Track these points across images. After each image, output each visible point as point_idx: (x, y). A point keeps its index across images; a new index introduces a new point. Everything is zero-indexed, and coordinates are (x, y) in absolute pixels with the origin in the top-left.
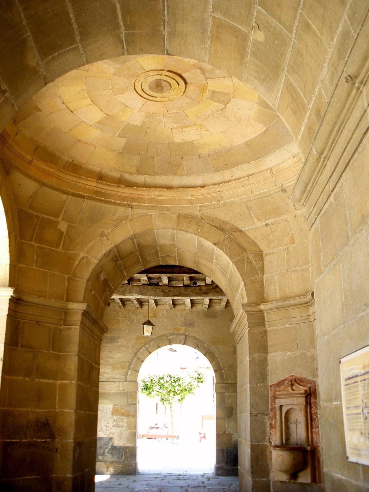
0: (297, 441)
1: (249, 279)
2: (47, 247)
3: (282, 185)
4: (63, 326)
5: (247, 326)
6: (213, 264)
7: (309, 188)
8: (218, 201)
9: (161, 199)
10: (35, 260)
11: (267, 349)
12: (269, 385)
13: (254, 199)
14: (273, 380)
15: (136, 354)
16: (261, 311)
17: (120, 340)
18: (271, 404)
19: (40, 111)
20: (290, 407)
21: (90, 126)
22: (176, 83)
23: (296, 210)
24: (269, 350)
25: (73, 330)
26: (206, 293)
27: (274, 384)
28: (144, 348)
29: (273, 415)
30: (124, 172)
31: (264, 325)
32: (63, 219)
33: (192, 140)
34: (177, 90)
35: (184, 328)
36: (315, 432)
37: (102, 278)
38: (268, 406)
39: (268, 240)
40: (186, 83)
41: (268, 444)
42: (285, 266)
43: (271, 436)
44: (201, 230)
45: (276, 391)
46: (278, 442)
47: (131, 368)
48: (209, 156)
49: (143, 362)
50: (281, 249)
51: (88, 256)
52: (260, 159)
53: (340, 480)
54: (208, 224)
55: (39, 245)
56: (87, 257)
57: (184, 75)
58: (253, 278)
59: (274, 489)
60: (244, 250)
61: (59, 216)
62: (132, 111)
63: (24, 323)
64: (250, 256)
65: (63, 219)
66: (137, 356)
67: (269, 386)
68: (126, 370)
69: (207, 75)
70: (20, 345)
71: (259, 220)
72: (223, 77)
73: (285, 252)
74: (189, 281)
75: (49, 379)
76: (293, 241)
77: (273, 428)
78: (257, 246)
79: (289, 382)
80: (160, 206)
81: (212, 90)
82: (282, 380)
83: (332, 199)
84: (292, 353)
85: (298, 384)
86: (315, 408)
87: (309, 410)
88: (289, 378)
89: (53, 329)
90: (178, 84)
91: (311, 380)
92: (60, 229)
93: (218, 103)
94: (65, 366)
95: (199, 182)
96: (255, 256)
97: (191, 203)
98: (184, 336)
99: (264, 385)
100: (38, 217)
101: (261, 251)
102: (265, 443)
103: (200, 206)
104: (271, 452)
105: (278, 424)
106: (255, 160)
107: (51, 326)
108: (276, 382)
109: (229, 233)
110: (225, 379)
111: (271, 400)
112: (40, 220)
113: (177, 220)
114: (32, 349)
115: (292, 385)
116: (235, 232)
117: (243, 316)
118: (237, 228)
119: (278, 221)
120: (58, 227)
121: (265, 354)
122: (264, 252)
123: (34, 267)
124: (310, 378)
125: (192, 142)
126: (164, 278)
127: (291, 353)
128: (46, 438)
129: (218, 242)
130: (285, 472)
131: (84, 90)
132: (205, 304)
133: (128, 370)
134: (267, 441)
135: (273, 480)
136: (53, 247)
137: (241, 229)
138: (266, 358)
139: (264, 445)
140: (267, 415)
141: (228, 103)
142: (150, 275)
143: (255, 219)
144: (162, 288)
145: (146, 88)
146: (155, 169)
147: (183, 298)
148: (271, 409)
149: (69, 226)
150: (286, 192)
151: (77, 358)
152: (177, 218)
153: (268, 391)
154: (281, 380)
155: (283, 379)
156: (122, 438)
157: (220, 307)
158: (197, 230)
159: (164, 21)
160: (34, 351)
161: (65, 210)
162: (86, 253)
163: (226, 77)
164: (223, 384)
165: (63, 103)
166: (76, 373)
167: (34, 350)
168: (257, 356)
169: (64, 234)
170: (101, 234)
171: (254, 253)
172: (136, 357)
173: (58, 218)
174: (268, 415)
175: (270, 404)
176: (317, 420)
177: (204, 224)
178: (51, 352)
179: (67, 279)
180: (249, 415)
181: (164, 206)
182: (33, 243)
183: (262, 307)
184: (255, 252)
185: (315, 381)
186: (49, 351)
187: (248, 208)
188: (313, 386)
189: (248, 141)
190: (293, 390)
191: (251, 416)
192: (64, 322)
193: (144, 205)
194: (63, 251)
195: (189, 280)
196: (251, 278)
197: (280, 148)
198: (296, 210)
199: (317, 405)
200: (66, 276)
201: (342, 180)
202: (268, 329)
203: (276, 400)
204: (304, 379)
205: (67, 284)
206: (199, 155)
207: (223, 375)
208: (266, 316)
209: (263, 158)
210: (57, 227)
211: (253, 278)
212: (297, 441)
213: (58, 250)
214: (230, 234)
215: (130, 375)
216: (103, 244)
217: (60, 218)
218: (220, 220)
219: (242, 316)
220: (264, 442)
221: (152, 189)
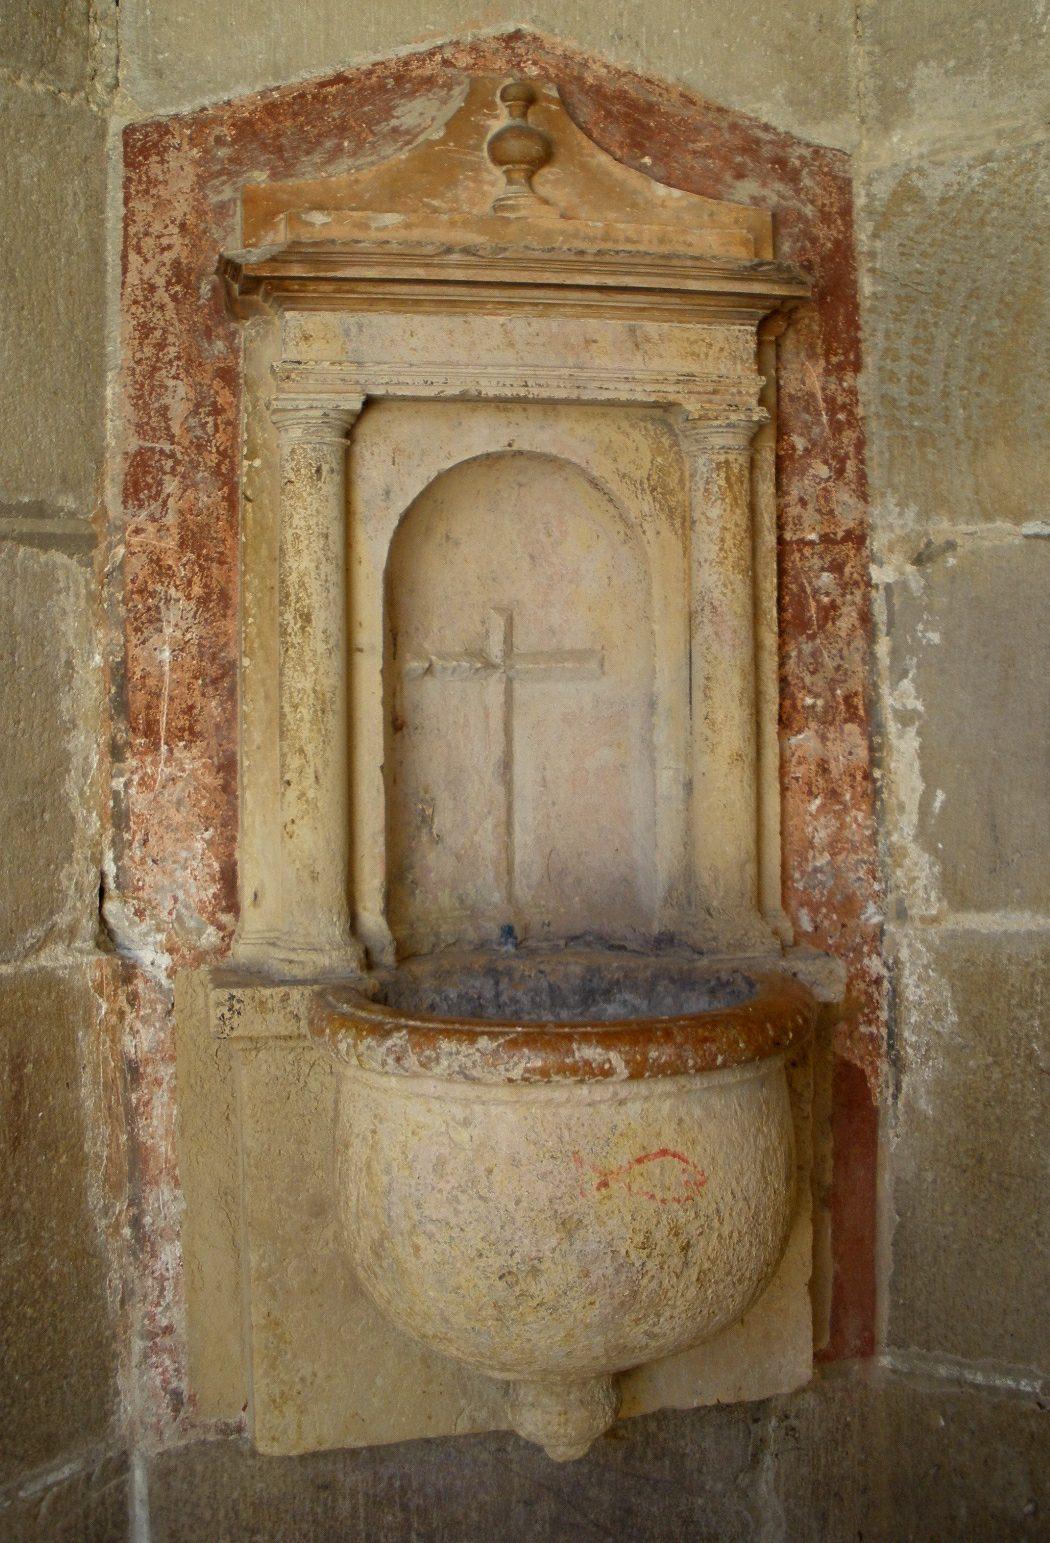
0: (510, 897)
27: (200, 123)
29: (171, 543)
36: (823, 768)
38: (95, 413)
43: (120, 846)
67: (114, 144)
77: (150, 730)
82: (340, 78)
86: (840, 472)
91: (789, 140)
99: (54, 96)
102: (44, 960)
108: (244, 92)
111: (145, 330)
124: (771, 111)
135: (173, 1441)
139: (48, 981)
140: (81, 544)
153: (97, 204)
154: (328, 72)
155: (360, 60)
174: (92, 541)
175: (114, 391)
176: (847, 620)
185: (844, 156)
188: (809, 211)
199: (860, 444)
204: (688, 113)
212: (510, 897)
220: (37, 948)
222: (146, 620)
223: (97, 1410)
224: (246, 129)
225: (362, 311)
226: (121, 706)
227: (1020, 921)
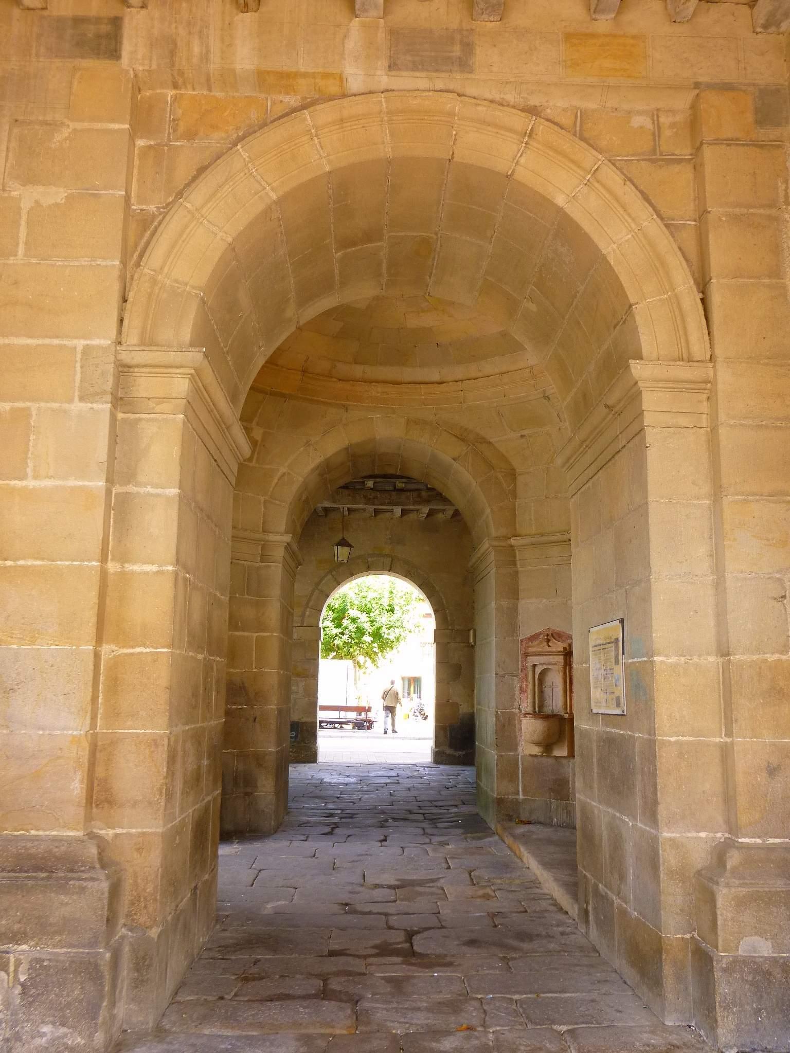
7: (571, 461)
14: (526, 632)
15: (318, 584)
16: (512, 546)
18: (522, 663)
20: (545, 667)
24: (521, 595)
26: (427, 501)
28: (330, 576)
31: (515, 565)
32: (258, 424)
38: (518, 665)
41: (517, 711)
45: (528, 647)
46: (529, 709)
53: (586, 730)
56: (289, 473)
59: (522, 764)
60: (491, 467)
64: (500, 476)
66: (320, 587)
71: (512, 430)
79: (544, 636)
83: (590, 484)
85: (555, 639)
87: (568, 671)
92: (253, 437)
94: (263, 614)
95: (436, 377)
101: (514, 470)
104: (521, 721)
105: (530, 687)
108: (529, 636)
115: (548, 641)
116: (481, 443)
122: (517, 470)
128: (242, 705)
130: (538, 744)
134: (516, 708)
138: (517, 605)
140: (517, 676)
148: (522, 669)
156: (297, 709)
157: (443, 516)
159: (431, 273)
164: (447, 631)
169: (259, 444)
172: (317, 589)
173: (252, 423)
178: (247, 596)
179: (262, 501)
180: (494, 675)
183: (512, 542)
190: (549, 646)
191: (496, 677)
194: (257, 465)
201: (599, 474)
202: (520, 569)
203: (528, 658)
205: (263, 509)
208: (517, 553)
213: (251, 465)
214: (474, 445)
216: (309, 456)
217: (254, 423)
218: (461, 427)
221: (374, 384)
222: (523, 682)
223: (516, 749)
224: (529, 639)
225: (736, 814)
226: (521, 690)
227: (787, 840)
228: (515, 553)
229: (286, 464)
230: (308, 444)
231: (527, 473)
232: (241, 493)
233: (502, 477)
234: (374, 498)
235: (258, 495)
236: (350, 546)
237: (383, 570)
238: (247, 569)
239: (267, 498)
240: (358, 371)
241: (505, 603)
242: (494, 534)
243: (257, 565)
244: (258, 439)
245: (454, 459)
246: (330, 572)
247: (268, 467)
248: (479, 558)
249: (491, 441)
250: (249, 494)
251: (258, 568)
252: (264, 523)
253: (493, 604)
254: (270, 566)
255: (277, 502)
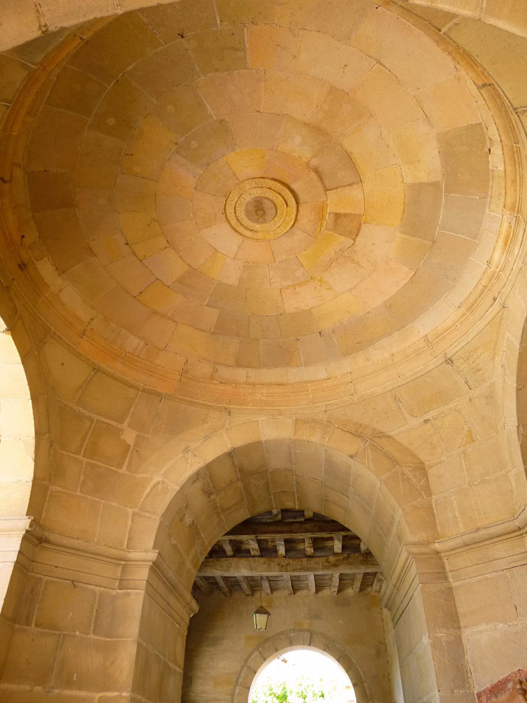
1: (409, 504)
2: (103, 465)
3: (445, 354)
4: (119, 591)
5: (417, 580)
6: (348, 497)
8: (351, 395)
9: (270, 400)
10: (81, 482)
11: (458, 621)
12: (475, 693)
13: (404, 383)
15: (246, 661)
16: (437, 553)
17: (225, 641)
19: (95, 255)
21: (168, 287)
22: (284, 202)
23: (471, 389)
25: (133, 597)
27: (485, 691)
28: (256, 653)
30: (218, 363)
31: (446, 578)
32: (130, 426)
33: (310, 307)
34: (285, 215)
35: (309, 621)
37: (188, 520)
39: (431, 444)
40: (297, 202)
42: (465, 479)
44: (329, 438)
47: (239, 684)
48: (334, 332)
49: (256, 673)
50: (453, 454)
51: (165, 481)
52: (407, 327)
54: (339, 430)
55: (90, 461)
56: (163, 482)
57: (294, 187)
58: (415, 503)
60: (395, 462)
61: (124, 421)
62: (224, 260)
63: (47, 582)
64: (407, 471)
65: (130, 426)
66: (248, 664)
67: (476, 696)
68: (232, 687)
69: (327, 182)
70: (34, 622)
71: (413, 416)
72: (349, 185)
73: (460, 458)
74: (312, 549)
75: (80, 689)
76: (472, 438)
78: (414, 456)
80: (270, 409)
81: (335, 211)
82: (499, 681)
84: (509, 626)
88: (514, 675)
89: (100, 595)
90: (287, 204)
93: (343, 237)
94: (113, 663)
96: (412, 469)
97: (312, 402)
98: (309, 634)
100: (91, 420)
101: (422, 463)
103: (326, 405)
106: (399, 330)
107: (97, 588)
108: (488, 685)
109: (370, 439)
110: (369, 697)
112: (94, 424)
113: (294, 426)
114: (56, 630)
116: (379, 437)
117: (406, 566)
118: (381, 433)
119: (443, 412)
120: (122, 437)
121: (457, 630)
122: (427, 463)
123: (78, 493)
125: (309, 312)
126: (279, 544)
127: (507, 626)
129: (356, 454)
131: (154, 220)
132: (333, 586)
133: (235, 686)
136: (113, 466)
137: (387, 434)
138: (460, 637)
141: (357, 235)
142: (261, 535)
143: (407, 416)
144: (278, 560)
145: (242, 215)
146: (261, 358)
147: (306, 573)
149: (138, 436)
150: (452, 363)
151: (135, 647)
152: (294, 423)
154: (497, 681)
155: (501, 678)
157: (352, 591)
158: (324, 438)
160: (60, 635)
161: (133, 413)
162: (162, 476)
163: (354, 184)
165: (127, 244)
166: (131, 677)
167: (59, 632)
168: (442, 635)
169: (131, 448)
170: (186, 448)
171: (412, 467)
173: (123, 423)
177: (333, 429)
178: (92, 636)
181: (275, 409)
182: (80, 457)
184: (412, 465)
186: (89, 634)
187: (396, 399)
189: (387, 301)
192: (120, 583)
193: (246, 408)
194: (128, 473)
195: (312, 547)
196: (412, 502)
197: (435, 302)
198: (471, 389)
200: (130, 510)
202: (453, 585)
205: (130, 523)
206: (320, 333)
207: (366, 692)
209: (410, 325)
210: (121, 437)
211: (415, 503)
213: (120, 471)
215: (238, 694)
217: (125, 424)
218: (356, 424)
219: (404, 567)
224: (490, 691)
228: (444, 563)
229: (162, 472)
230: (187, 450)
231: (440, 463)
232: (102, 501)
233: (410, 472)
234: (287, 565)
235: (125, 506)
236: (266, 613)
237: (304, 644)
238: (97, 597)
239: (136, 510)
240: (241, 374)
241: (442, 634)
242: (410, 538)
243: (114, 592)
244: (130, 444)
245: (351, 457)
246: (257, 648)
247: (141, 475)
248: (395, 586)
249: (391, 434)
250: (114, 504)
251: (115, 597)
252: (129, 539)
253: (426, 640)
254: (128, 594)
255: (148, 515)
